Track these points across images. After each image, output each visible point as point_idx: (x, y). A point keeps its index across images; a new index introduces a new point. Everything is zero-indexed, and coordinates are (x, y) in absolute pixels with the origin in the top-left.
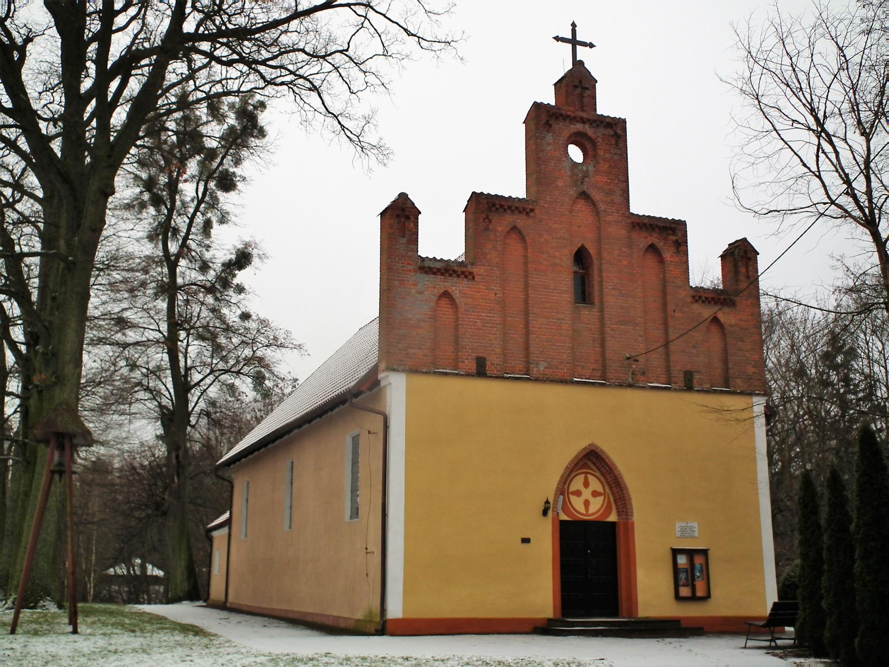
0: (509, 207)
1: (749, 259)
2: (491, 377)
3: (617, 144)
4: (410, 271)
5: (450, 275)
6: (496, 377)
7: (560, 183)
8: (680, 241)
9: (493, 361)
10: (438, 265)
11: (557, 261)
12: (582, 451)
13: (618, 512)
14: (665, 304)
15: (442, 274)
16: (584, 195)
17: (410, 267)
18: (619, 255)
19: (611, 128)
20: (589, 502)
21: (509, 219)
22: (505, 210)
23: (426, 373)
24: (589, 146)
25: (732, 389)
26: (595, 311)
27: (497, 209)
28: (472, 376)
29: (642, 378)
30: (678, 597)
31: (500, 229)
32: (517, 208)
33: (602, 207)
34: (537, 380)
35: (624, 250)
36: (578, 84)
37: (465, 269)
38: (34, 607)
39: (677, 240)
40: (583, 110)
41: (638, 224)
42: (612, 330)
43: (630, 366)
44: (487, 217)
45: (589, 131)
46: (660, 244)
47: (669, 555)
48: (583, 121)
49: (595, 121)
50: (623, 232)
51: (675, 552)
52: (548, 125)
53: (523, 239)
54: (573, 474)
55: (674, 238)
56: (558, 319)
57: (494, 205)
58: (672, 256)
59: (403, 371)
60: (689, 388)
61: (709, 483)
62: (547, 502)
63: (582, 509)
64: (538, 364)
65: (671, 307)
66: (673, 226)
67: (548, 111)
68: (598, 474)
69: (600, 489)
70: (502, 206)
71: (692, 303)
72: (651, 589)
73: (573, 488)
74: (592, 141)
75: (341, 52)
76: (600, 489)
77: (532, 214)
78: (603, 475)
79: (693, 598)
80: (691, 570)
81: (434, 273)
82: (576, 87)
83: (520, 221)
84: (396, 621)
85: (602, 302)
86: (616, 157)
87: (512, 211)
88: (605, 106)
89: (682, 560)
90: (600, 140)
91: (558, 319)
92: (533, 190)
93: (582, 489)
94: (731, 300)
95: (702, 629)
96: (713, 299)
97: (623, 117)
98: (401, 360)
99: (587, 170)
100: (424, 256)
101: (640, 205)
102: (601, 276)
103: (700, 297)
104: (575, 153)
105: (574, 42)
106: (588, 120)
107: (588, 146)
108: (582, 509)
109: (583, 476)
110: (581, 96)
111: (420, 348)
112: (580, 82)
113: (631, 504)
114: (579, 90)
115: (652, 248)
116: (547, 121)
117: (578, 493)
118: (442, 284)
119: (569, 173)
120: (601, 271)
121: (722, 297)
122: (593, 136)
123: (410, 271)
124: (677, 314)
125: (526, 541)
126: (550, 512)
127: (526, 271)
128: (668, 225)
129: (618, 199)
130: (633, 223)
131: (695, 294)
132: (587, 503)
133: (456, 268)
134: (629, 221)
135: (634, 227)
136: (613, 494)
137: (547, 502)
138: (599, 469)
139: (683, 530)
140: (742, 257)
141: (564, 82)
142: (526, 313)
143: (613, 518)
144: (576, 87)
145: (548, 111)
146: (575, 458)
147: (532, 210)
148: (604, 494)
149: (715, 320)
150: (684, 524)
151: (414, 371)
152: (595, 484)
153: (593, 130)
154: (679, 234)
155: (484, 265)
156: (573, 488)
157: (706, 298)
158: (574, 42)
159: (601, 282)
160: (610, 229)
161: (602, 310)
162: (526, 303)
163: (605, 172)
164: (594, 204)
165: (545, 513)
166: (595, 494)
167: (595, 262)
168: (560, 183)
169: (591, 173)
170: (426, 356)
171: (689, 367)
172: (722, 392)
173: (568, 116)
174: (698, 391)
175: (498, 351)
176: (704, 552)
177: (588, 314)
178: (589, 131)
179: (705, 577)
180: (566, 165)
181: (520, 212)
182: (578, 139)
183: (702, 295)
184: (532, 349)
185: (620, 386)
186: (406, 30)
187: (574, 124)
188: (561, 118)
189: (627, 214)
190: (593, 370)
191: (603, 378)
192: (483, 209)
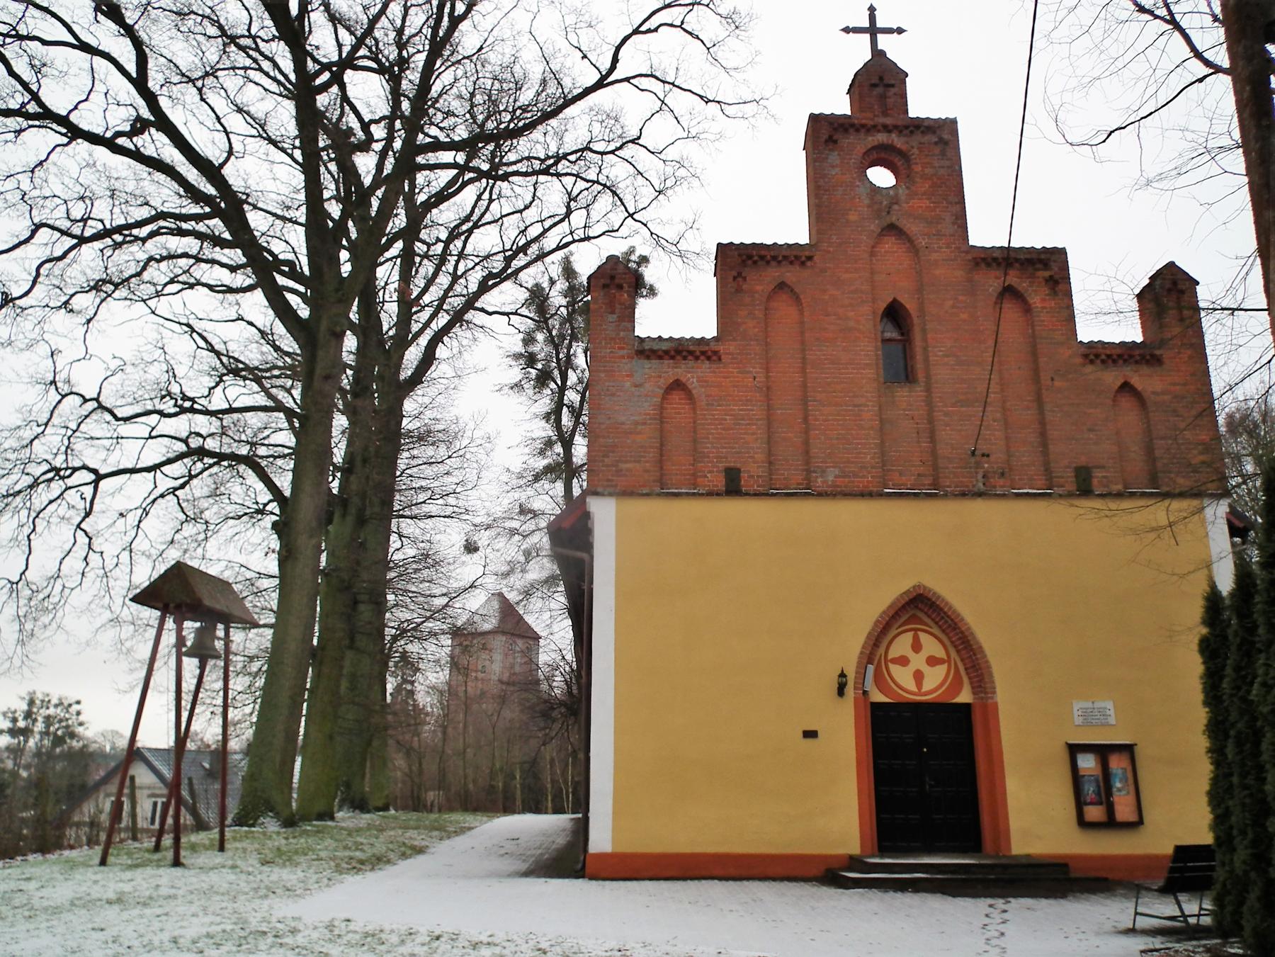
0: (774, 258)
1: (946, 143)
2: (747, 494)
3: (943, 153)
4: (623, 357)
5: (685, 358)
6: (755, 495)
7: (853, 217)
8: (1057, 277)
9: (753, 472)
10: (665, 346)
11: (851, 324)
12: (901, 595)
13: (973, 688)
14: (1036, 371)
15: (672, 358)
16: (892, 229)
17: (622, 352)
18: (953, 307)
19: (934, 132)
20: (921, 673)
21: (773, 274)
22: (768, 262)
23: (647, 495)
24: (899, 162)
25: (1165, 489)
26: (919, 390)
27: (755, 262)
28: (718, 495)
29: (1001, 481)
30: (1083, 823)
31: (759, 288)
32: (785, 257)
33: (922, 242)
34: (821, 495)
35: (961, 298)
36: (879, 82)
37: (706, 348)
38: (253, 825)
39: (1051, 277)
40: (885, 114)
41: (984, 259)
42: (946, 414)
43: (978, 465)
44: (740, 274)
45: (897, 141)
46: (1022, 285)
47: (1064, 756)
48: (887, 129)
49: (907, 127)
50: (959, 273)
51: (1074, 750)
52: (831, 141)
53: (797, 299)
54: (893, 632)
55: (1047, 274)
56: (855, 406)
57: (750, 257)
58: (1043, 300)
59: (610, 495)
60: (1085, 490)
61: (1089, 636)
62: (842, 675)
63: (910, 685)
64: (824, 472)
65: (1045, 378)
66: (1043, 256)
67: (831, 124)
68: (936, 631)
69: (939, 652)
70: (762, 258)
71: (1084, 365)
72: (1035, 813)
73: (894, 652)
74: (900, 153)
75: (633, 141)
76: (939, 652)
77: (809, 263)
78: (943, 631)
79: (1111, 823)
80: (1102, 778)
81: (660, 358)
82: (874, 85)
83: (790, 274)
84: (602, 856)
85: (928, 377)
86: (942, 172)
87: (779, 262)
88: (920, 105)
89: (1087, 763)
90: (915, 151)
91: (855, 406)
92: (819, 232)
93: (924, 654)
94: (1152, 356)
95: (1106, 879)
96: (1120, 356)
97: (952, 116)
98: (608, 480)
99: (897, 195)
100: (643, 335)
101: (985, 231)
102: (925, 340)
103: (1097, 356)
104: (881, 177)
105: (873, 30)
106: (896, 127)
107: (899, 164)
108: (910, 685)
109: (910, 634)
110: (883, 97)
111: (639, 462)
112: (881, 79)
113: (991, 675)
114: (880, 90)
115: (1009, 292)
116: (831, 137)
117: (903, 661)
118: (671, 371)
119: (867, 202)
120: (924, 331)
121: (1137, 352)
122: (904, 148)
123: (623, 357)
124: (1057, 383)
125: (810, 734)
126: (850, 690)
127: (803, 342)
128: (1034, 256)
129: (948, 227)
130: (974, 258)
131: (1087, 351)
132: (919, 676)
133: (691, 348)
134: (969, 257)
135: (977, 264)
136: (962, 660)
137: (842, 675)
138: (936, 623)
139: (1086, 713)
140: (1169, 290)
141: (857, 84)
142: (805, 401)
143: (965, 697)
144: (874, 85)
145: (831, 124)
146: (890, 607)
147: (810, 258)
148: (949, 661)
149: (1126, 387)
150: (1090, 705)
151: (626, 493)
152: (931, 646)
153: (903, 139)
154: (1055, 267)
155: (734, 340)
156: (894, 652)
157: (1109, 356)
158: (873, 30)
159: (925, 349)
160: (937, 272)
161: (928, 390)
162: (804, 386)
163: (924, 194)
164: (910, 240)
165: (841, 691)
166: (932, 661)
167: (916, 320)
168: (853, 217)
169: (903, 198)
170: (646, 471)
171: (1083, 461)
172: (1144, 495)
173: (863, 126)
174: (1102, 496)
175: (760, 457)
176: (1128, 749)
177: (903, 394)
178: (897, 141)
179: (1132, 788)
180: (862, 191)
181: (791, 263)
182: (883, 155)
183: (1102, 354)
184: (814, 451)
185: (963, 495)
186: (701, 97)
187: (879, 138)
188: (851, 130)
189: (964, 248)
190: (919, 475)
191: (933, 488)
192: (737, 263)
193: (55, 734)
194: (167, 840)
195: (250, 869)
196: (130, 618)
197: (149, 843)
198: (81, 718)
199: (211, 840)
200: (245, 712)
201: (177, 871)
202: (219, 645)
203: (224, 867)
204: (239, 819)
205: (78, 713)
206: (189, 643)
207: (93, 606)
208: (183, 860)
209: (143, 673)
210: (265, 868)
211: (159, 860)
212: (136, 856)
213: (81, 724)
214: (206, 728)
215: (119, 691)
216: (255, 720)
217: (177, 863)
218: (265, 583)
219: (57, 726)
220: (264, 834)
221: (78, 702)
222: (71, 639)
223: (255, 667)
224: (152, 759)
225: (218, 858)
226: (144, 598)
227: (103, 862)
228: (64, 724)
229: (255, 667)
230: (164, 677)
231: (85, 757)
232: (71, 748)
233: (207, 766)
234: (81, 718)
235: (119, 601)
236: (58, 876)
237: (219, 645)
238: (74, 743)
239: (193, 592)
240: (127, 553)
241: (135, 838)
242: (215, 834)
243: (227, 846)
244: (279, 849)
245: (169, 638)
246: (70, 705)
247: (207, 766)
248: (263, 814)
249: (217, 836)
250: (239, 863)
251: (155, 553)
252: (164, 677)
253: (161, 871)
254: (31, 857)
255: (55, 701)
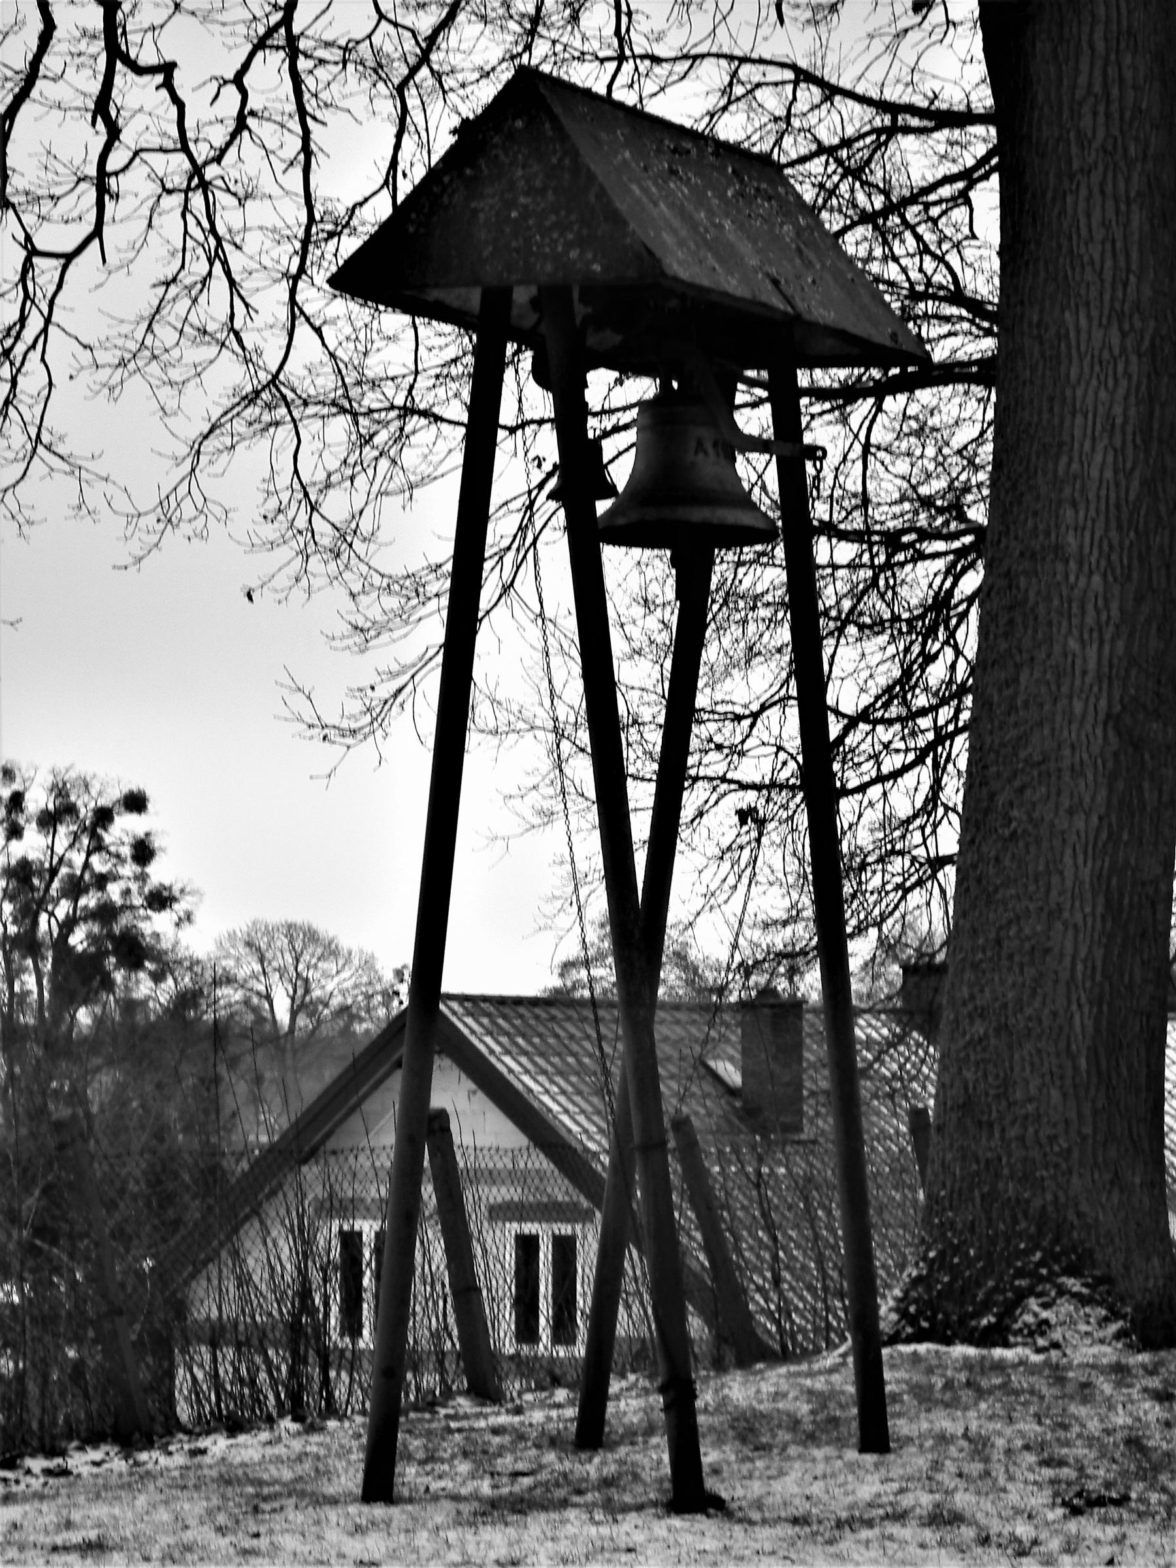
38: (997, 1336)
193: (61, 944)
194: (631, 1401)
195: (1023, 1530)
196: (326, 382)
197: (559, 1410)
198: (159, 873)
199: (821, 1399)
200: (908, 805)
201: (697, 1533)
202: (757, 473)
203: (900, 1516)
204: (929, 1307)
205: (143, 852)
206: (620, 473)
207: (165, 334)
208: (711, 1484)
209: (433, 630)
210: (1089, 1527)
211: (607, 1483)
212: (506, 1463)
213: (160, 900)
214: (731, 906)
215: (326, 732)
216: (948, 840)
217: (689, 1494)
218: (917, 159)
219: (63, 909)
220: (1057, 1375)
221: (136, 802)
222: (93, 497)
223: (919, 581)
224: (486, 1045)
225: (868, 1483)
226: (389, 271)
227: (379, 1486)
228: (89, 901)
229: (919, 581)
230: (523, 656)
231: (201, 1038)
232: (130, 1006)
233: (732, 1074)
234: (159, 873)
235: (271, 301)
236: (203, 1534)
237: (757, 473)
238: (144, 987)
239: (617, 220)
240: (276, 59)
241: (485, 1390)
242: (834, 1370)
243: (899, 1426)
244: (1134, 1443)
245: (524, 463)
246: (104, 816)
247: (732, 1074)
248: (1037, 1283)
249: (846, 1383)
250: (963, 1500)
251: (396, 47)
252: (523, 656)
253: (630, 1529)
254: (80, 1461)
255: (38, 800)
